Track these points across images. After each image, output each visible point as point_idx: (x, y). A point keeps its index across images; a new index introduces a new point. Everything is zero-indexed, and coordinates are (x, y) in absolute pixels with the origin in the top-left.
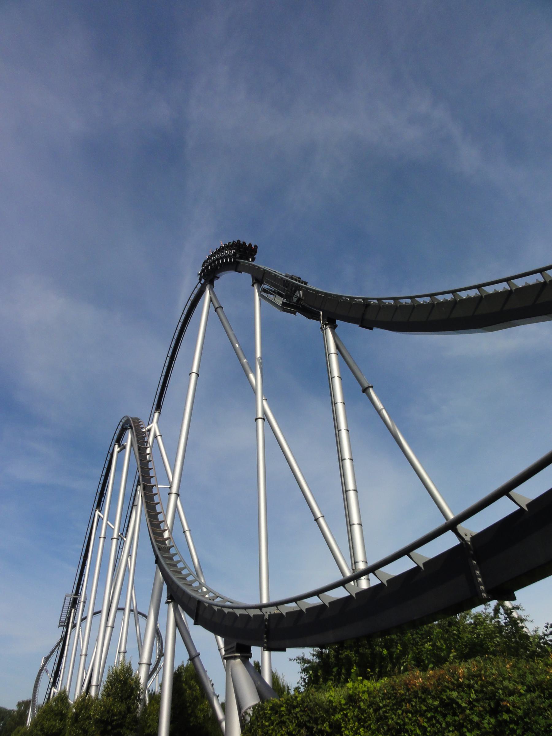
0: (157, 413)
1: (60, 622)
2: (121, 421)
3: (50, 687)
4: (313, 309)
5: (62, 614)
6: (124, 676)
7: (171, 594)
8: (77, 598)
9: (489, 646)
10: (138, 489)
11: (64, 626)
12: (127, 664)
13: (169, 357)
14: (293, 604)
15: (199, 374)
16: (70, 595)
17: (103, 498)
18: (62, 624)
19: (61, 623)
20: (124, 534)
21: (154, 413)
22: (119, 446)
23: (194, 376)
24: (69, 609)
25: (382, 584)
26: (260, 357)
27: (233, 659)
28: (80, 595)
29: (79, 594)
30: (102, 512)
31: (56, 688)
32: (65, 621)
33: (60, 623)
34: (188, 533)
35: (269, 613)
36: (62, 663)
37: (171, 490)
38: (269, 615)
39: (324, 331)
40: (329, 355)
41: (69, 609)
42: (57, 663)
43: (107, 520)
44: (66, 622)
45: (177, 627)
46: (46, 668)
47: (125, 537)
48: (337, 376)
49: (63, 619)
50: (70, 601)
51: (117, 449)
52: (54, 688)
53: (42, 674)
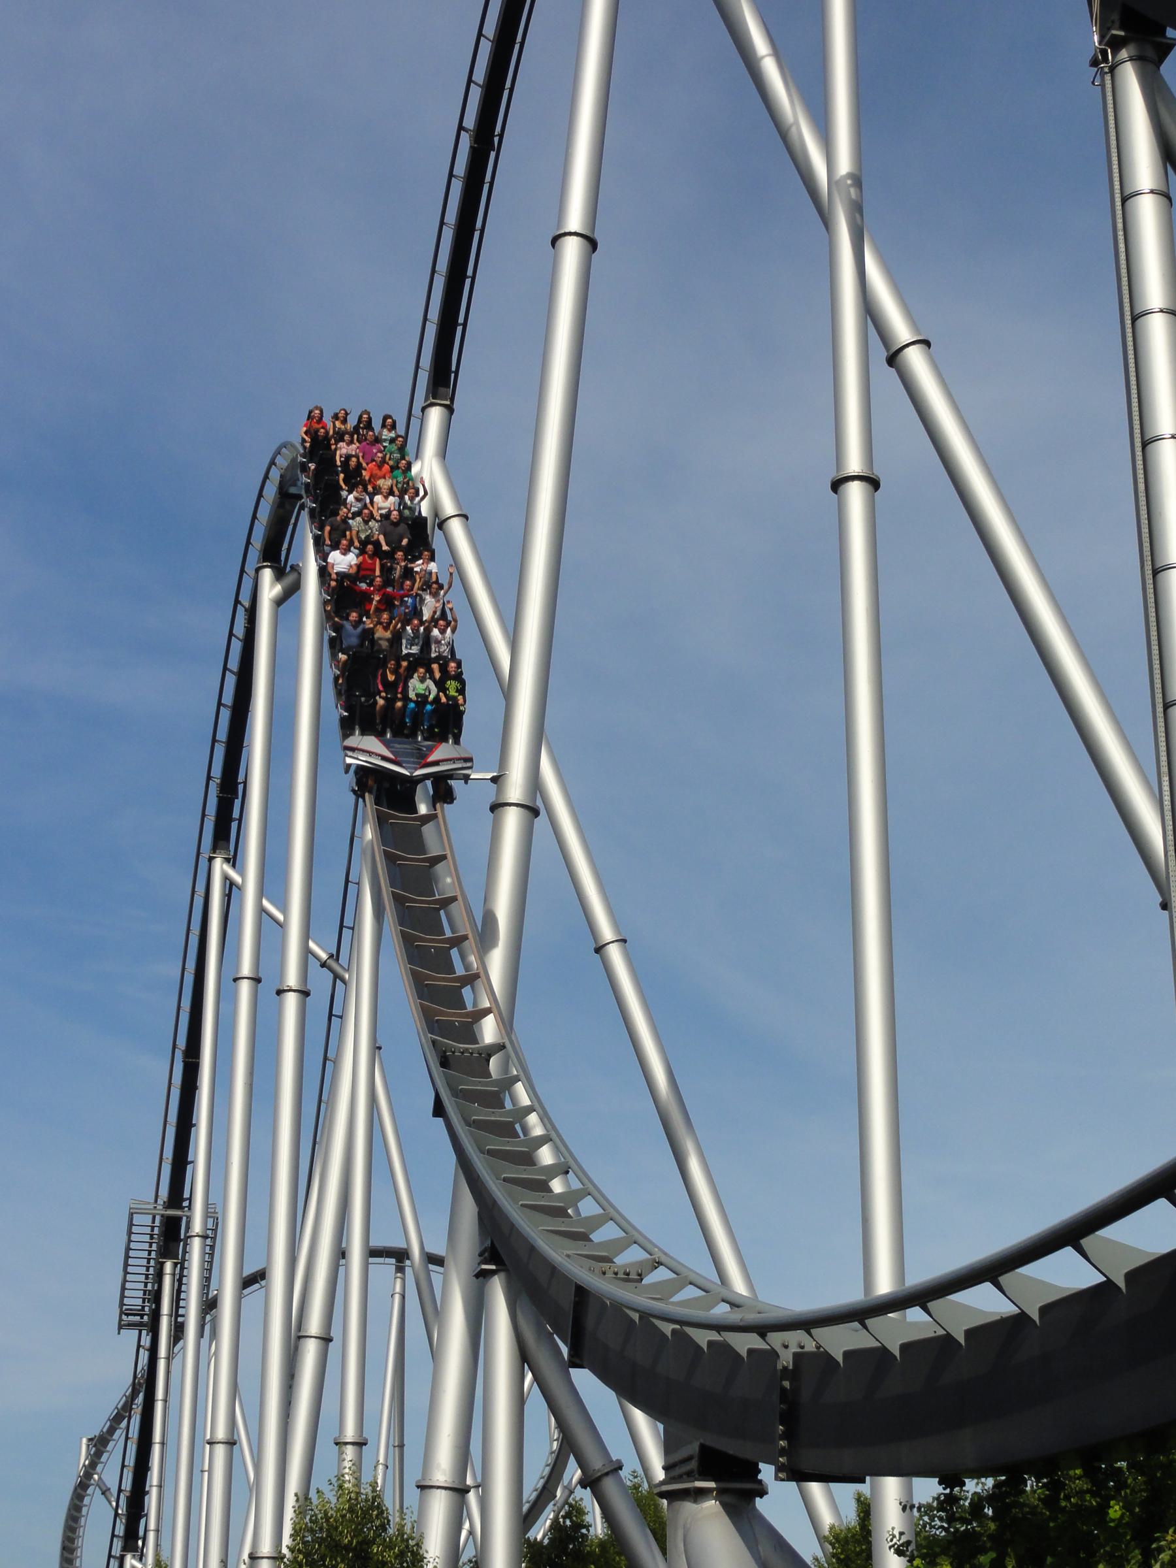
0: (438, 407)
1: (122, 1313)
2: (273, 463)
3: (117, 1551)
4: (190, 1060)
5: (125, 1281)
6: (357, 1533)
7: (492, 1243)
8: (178, 1220)
9: (858, 1549)
11: (138, 1325)
12: (366, 1490)
14: (915, 1314)
15: (597, 236)
16: (152, 1207)
17: (237, 803)
18: (131, 1318)
19: (127, 1315)
20: (343, 959)
21: (423, 409)
22: (279, 575)
23: (572, 249)
24: (152, 1263)
25: (1109, 1284)
26: (850, 175)
27: (690, 1501)
28: (190, 1207)
29: (186, 1204)
30: (237, 867)
31: (141, 1560)
32: (143, 1307)
34: (615, 954)
35: (794, 1349)
36: (150, 1465)
37: (500, 791)
38: (796, 1356)
39: (1108, 78)
40: (1124, 200)
41: (152, 1263)
42: (132, 1464)
43: (261, 893)
44: (147, 1309)
45: (525, 1364)
46: (100, 1478)
47: (348, 970)
48: (1162, 306)
49: (135, 1299)
50: (153, 1228)
51: (269, 588)
52: (134, 1557)
53: (86, 1500)
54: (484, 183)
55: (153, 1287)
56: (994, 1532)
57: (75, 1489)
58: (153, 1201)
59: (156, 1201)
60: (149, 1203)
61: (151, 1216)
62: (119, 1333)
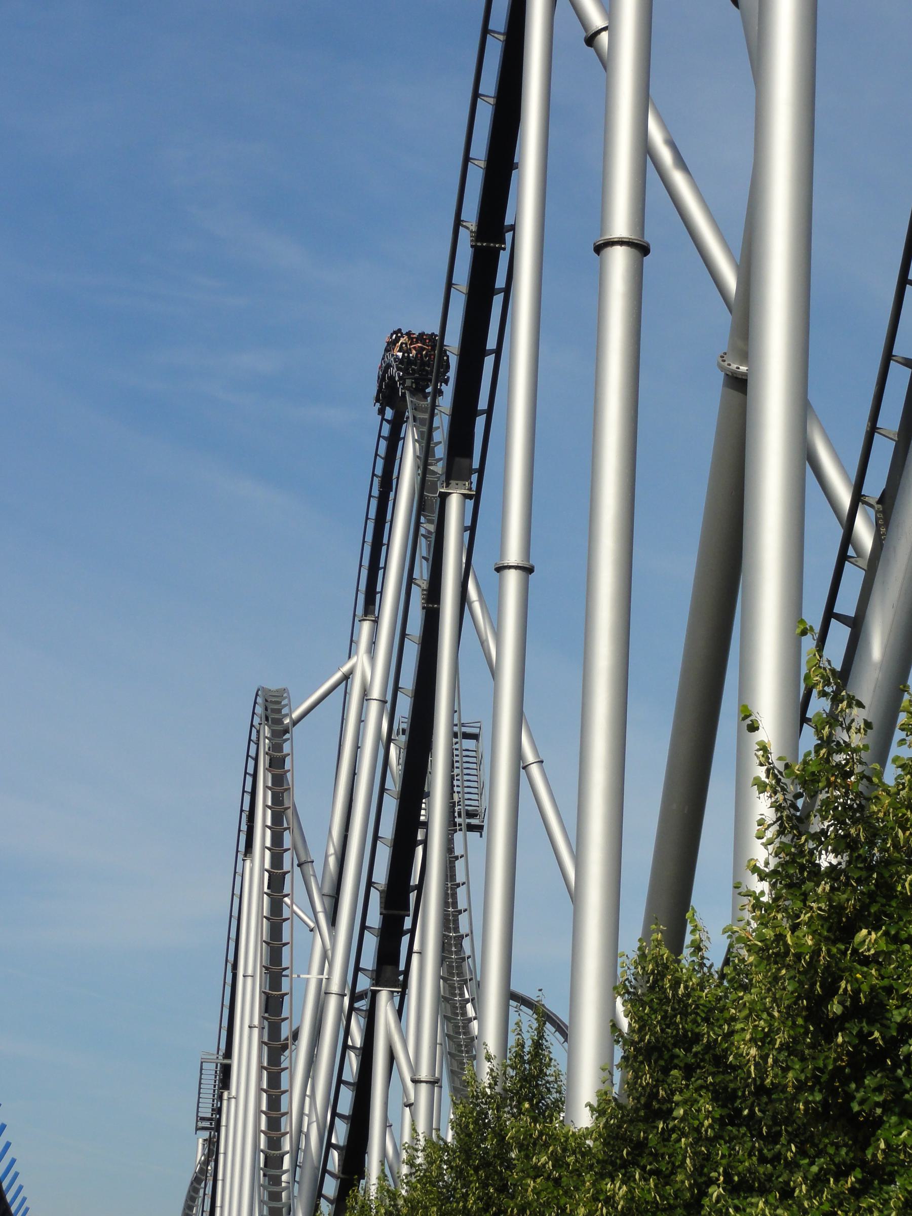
0: (368, 622)
10: (337, 858)
13: (377, 476)
33: (197, 1121)
49: (206, 1112)
54: (389, 501)
55: (216, 1116)
56: (714, 1095)
57: (192, 1183)
58: (216, 1052)
59: (218, 1053)
60: (213, 1055)
61: (215, 1064)
62: (196, 1134)
